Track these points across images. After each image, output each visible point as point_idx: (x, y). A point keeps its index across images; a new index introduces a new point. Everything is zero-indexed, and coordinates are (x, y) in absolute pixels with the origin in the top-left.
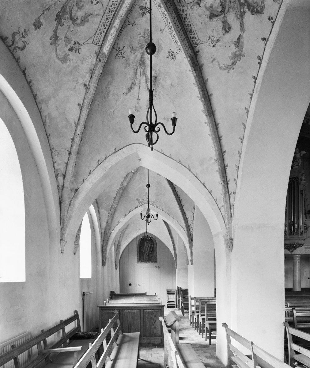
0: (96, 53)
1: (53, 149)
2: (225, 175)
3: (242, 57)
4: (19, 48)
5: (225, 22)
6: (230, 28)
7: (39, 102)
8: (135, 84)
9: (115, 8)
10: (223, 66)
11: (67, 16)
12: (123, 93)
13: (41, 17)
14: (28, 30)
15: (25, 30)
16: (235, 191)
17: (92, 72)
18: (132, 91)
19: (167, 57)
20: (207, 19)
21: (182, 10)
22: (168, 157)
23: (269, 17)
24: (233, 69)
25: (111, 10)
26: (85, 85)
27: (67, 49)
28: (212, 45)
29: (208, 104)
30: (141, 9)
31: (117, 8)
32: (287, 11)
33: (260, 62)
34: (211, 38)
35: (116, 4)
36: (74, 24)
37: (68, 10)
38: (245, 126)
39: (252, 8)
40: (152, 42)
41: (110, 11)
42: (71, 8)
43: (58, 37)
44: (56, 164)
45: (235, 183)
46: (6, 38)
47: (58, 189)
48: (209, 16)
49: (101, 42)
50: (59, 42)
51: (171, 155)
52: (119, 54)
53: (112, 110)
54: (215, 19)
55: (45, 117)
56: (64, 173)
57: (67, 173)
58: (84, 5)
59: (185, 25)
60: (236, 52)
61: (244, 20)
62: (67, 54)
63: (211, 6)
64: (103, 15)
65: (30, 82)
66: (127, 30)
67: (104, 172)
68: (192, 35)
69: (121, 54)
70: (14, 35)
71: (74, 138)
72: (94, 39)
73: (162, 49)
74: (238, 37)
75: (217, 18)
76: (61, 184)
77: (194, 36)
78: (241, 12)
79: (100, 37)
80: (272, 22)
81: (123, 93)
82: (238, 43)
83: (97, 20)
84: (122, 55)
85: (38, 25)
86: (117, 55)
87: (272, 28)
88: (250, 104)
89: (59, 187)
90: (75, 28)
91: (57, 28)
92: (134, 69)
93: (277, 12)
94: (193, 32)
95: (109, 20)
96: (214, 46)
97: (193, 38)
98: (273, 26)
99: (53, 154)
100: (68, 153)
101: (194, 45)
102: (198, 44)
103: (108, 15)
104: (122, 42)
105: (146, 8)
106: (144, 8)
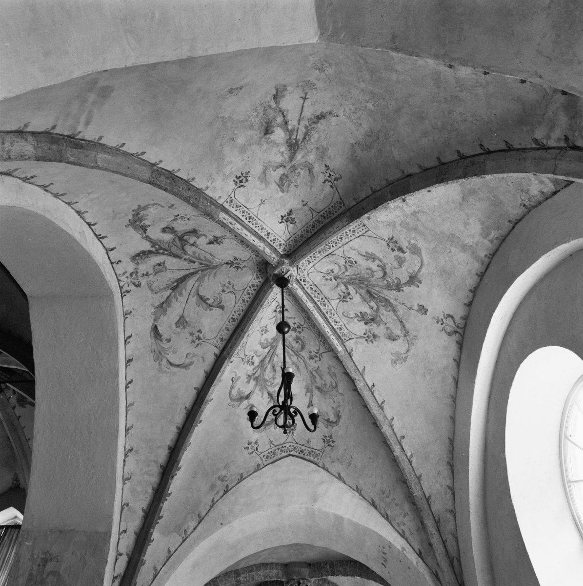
4: (454, 322)
30: (293, 219)
55: (491, 241)
64: (345, 244)
72: (366, 232)
78: (157, 245)
81: (337, 116)
84: (328, 171)
92: (309, 140)
104: (325, 192)
106: (289, 220)
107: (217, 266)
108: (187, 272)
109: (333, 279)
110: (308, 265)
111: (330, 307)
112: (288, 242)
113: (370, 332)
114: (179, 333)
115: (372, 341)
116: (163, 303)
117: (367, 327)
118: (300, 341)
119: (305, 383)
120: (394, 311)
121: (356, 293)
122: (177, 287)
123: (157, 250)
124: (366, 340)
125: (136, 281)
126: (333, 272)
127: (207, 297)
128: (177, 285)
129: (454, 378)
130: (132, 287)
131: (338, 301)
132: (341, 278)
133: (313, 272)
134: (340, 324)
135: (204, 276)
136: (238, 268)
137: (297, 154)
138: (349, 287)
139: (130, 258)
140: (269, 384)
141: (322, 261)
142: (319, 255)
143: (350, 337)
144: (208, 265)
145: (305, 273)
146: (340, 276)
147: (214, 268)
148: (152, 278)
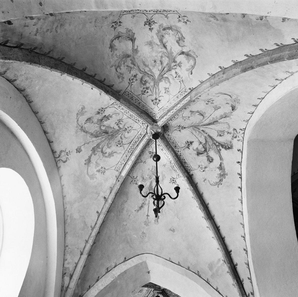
0: (116, 176)
1: (67, 246)
2: (237, 275)
3: (226, 176)
4: (62, 161)
5: (208, 157)
6: (212, 160)
7: (65, 203)
8: (145, 204)
9: (132, 150)
10: (213, 183)
11: (100, 150)
12: (135, 211)
13: (82, 147)
14: (72, 152)
15: (69, 151)
16: (252, 292)
17: (112, 189)
18: (142, 209)
19: (170, 183)
20: (195, 156)
21: (177, 151)
22: (177, 264)
23: (238, 150)
24: (221, 184)
25: (129, 151)
26: (105, 198)
27: (95, 170)
28: (202, 171)
29: (207, 211)
30: (150, 153)
31: (134, 151)
32: (248, 142)
33: (240, 177)
34: (200, 166)
35: (133, 148)
36: (103, 156)
37: (101, 147)
38: (244, 225)
39: (224, 147)
40: (156, 162)
41: (128, 152)
42: (103, 146)
43: (90, 161)
44: (66, 262)
45: (250, 282)
46: (56, 152)
47: (62, 291)
48: (196, 154)
49: (121, 170)
50: (91, 165)
51: (179, 263)
52: (133, 181)
53: (125, 223)
54: (201, 155)
55: (68, 216)
56: (72, 273)
57: (75, 273)
58: (112, 146)
59: (181, 159)
60: (220, 173)
61: (221, 154)
62: (95, 173)
63: (197, 148)
64: (124, 154)
65: (63, 185)
66: (140, 165)
67: (112, 279)
68: (187, 165)
69: (135, 181)
70: (61, 151)
71: (88, 240)
72: (116, 168)
73: (165, 178)
74: (220, 164)
75: (202, 155)
76: (66, 285)
77: (188, 165)
78: (218, 150)
79: (121, 167)
80: (240, 152)
81: (135, 211)
82: (221, 167)
83: (120, 156)
84: (135, 182)
85: (79, 150)
86: (132, 181)
87: (242, 155)
88: (242, 208)
89: (63, 288)
90: (104, 158)
91: (91, 155)
93: (242, 146)
94: (187, 163)
95: (128, 157)
96: (203, 171)
97: (187, 167)
98: (242, 154)
99: (66, 251)
100: (79, 253)
101: (189, 171)
102: (191, 170)
103: (127, 154)
105: (153, 152)
107: (191, 127)
108: (207, 126)
109: (127, 128)
110: (142, 132)
111: (127, 115)
112: (152, 143)
113: (101, 113)
114: (220, 104)
115: (99, 110)
116: (224, 118)
117: (104, 115)
118: (144, 83)
119: (139, 54)
120: (92, 134)
121: (113, 127)
122: (215, 122)
123: (218, 146)
124: (103, 108)
125: (235, 132)
126: (128, 132)
127: (199, 116)
128: (215, 122)
129: (48, 133)
130: (238, 131)
131: (123, 119)
132: (123, 131)
133: (138, 129)
134: (120, 109)
135: (199, 123)
136: (179, 126)
137: (149, 185)
138: (118, 128)
139: (233, 148)
140: (165, 54)
141: (134, 136)
142: (136, 140)
143: (113, 105)
144: (195, 127)
145: (142, 127)
146: (123, 131)
147: (192, 126)
148: (227, 130)
